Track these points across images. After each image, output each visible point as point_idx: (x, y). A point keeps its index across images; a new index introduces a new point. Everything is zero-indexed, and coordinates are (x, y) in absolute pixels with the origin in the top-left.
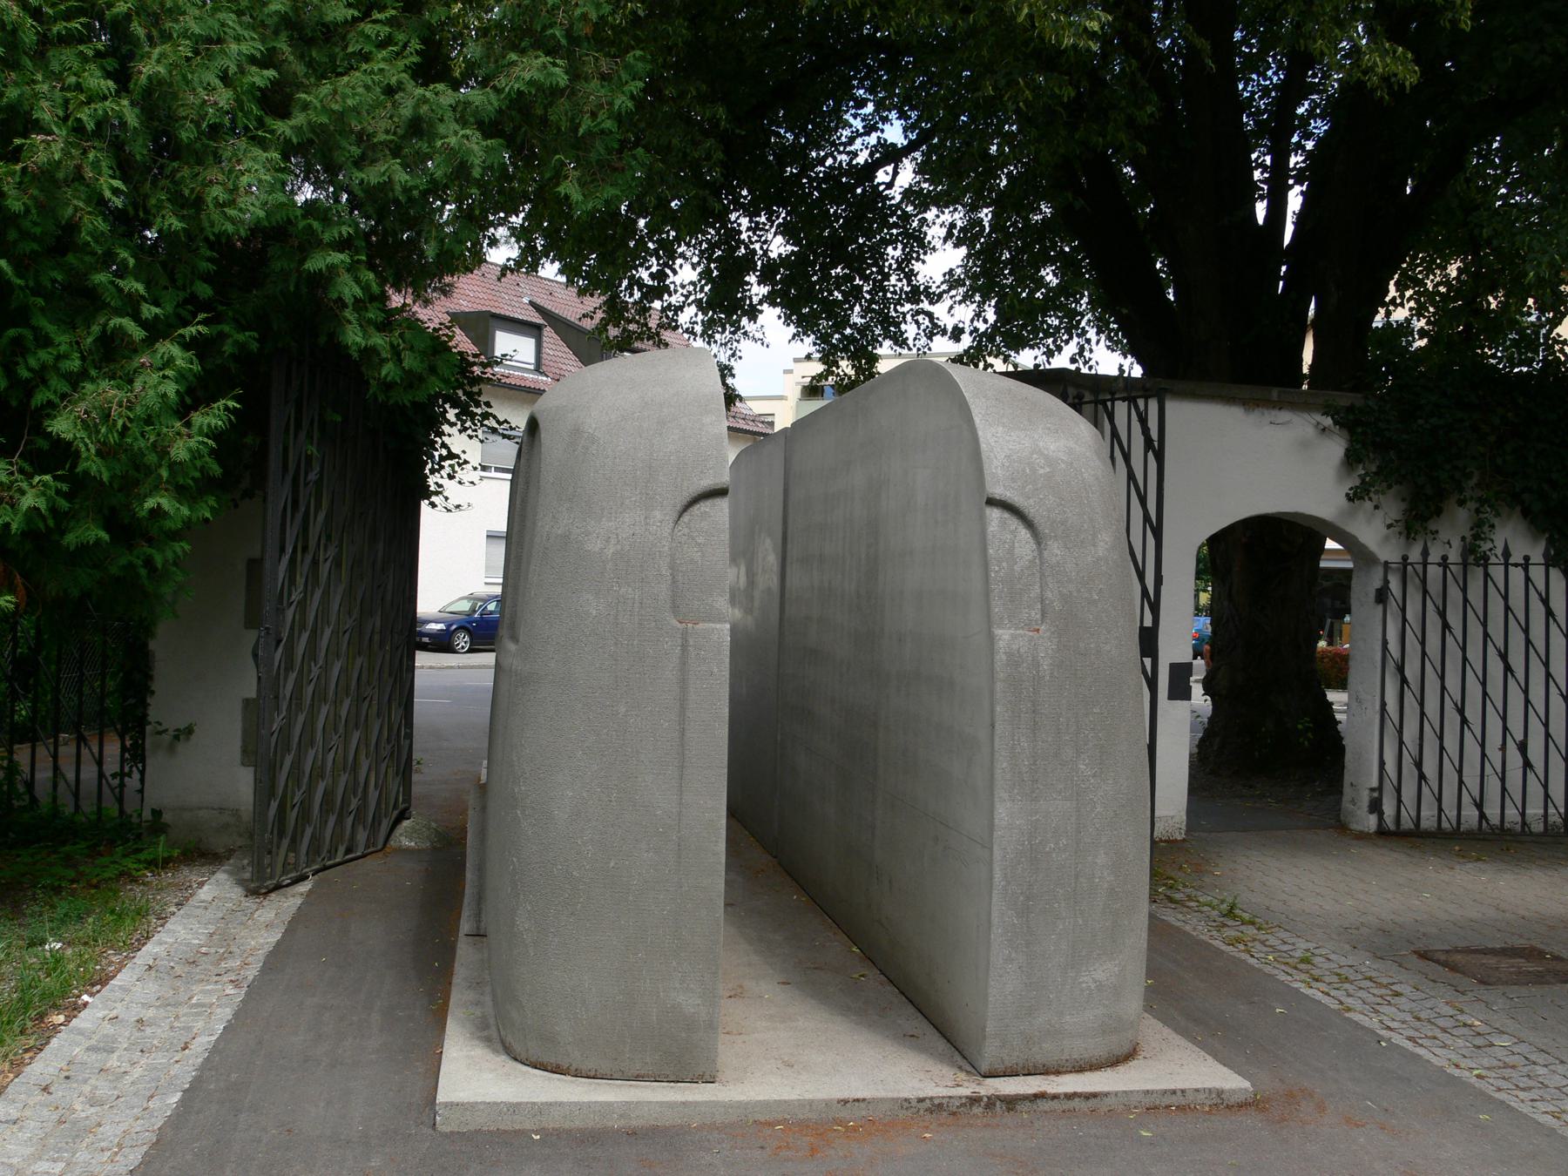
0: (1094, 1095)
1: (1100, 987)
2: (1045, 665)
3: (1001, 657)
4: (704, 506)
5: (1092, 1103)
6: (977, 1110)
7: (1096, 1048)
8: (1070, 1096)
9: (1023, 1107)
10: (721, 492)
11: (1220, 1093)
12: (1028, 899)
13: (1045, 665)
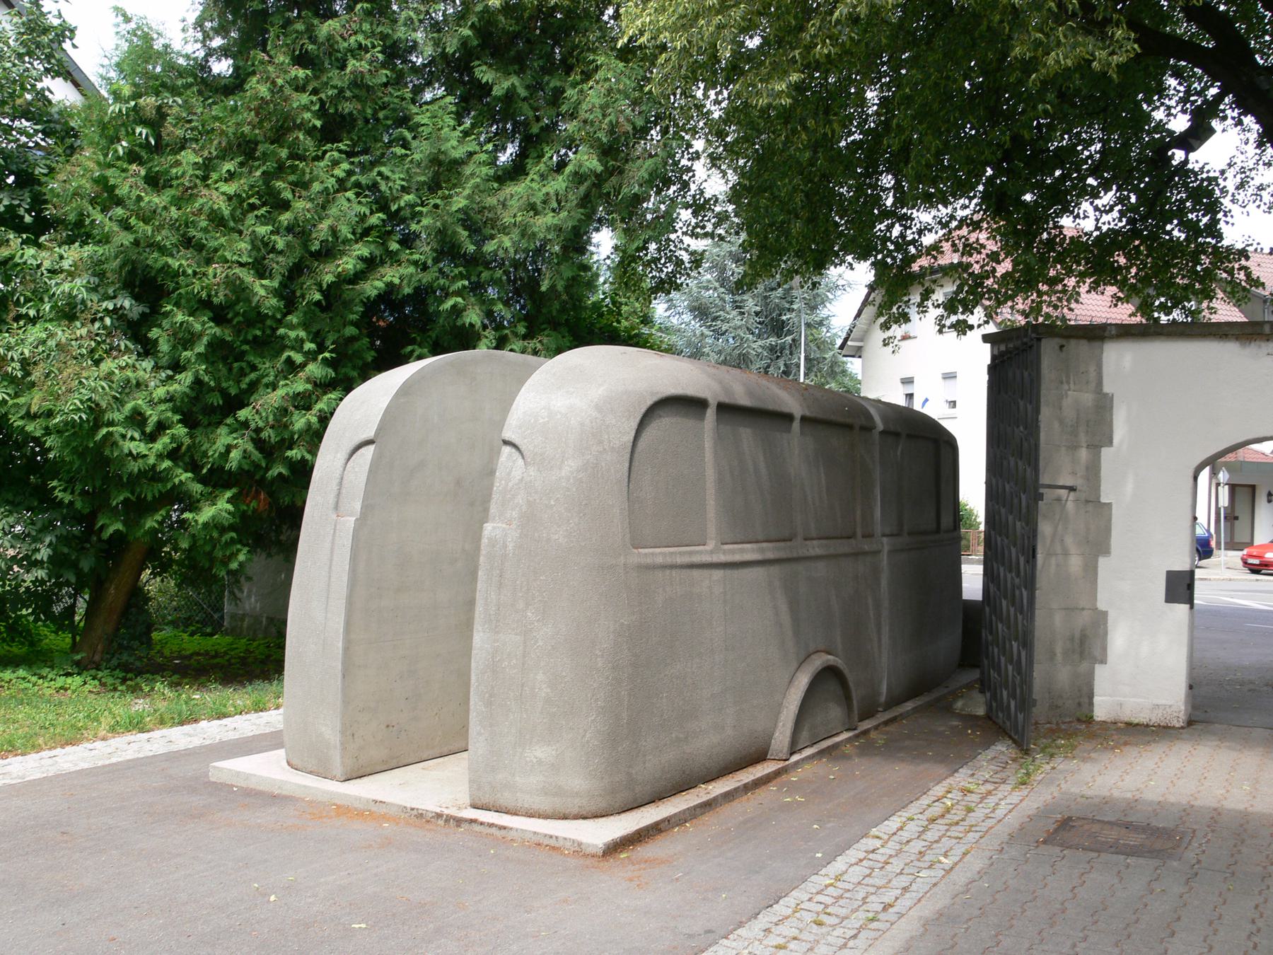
0: (505, 828)
1: (540, 762)
2: (510, 546)
3: (485, 541)
4: (362, 450)
5: (503, 832)
6: (441, 822)
7: (544, 804)
8: (491, 825)
9: (465, 826)
10: (369, 442)
11: (580, 844)
12: (491, 696)
13: (510, 546)
